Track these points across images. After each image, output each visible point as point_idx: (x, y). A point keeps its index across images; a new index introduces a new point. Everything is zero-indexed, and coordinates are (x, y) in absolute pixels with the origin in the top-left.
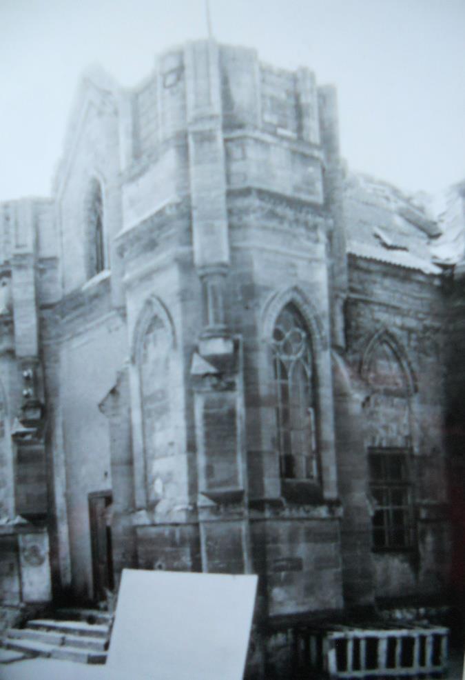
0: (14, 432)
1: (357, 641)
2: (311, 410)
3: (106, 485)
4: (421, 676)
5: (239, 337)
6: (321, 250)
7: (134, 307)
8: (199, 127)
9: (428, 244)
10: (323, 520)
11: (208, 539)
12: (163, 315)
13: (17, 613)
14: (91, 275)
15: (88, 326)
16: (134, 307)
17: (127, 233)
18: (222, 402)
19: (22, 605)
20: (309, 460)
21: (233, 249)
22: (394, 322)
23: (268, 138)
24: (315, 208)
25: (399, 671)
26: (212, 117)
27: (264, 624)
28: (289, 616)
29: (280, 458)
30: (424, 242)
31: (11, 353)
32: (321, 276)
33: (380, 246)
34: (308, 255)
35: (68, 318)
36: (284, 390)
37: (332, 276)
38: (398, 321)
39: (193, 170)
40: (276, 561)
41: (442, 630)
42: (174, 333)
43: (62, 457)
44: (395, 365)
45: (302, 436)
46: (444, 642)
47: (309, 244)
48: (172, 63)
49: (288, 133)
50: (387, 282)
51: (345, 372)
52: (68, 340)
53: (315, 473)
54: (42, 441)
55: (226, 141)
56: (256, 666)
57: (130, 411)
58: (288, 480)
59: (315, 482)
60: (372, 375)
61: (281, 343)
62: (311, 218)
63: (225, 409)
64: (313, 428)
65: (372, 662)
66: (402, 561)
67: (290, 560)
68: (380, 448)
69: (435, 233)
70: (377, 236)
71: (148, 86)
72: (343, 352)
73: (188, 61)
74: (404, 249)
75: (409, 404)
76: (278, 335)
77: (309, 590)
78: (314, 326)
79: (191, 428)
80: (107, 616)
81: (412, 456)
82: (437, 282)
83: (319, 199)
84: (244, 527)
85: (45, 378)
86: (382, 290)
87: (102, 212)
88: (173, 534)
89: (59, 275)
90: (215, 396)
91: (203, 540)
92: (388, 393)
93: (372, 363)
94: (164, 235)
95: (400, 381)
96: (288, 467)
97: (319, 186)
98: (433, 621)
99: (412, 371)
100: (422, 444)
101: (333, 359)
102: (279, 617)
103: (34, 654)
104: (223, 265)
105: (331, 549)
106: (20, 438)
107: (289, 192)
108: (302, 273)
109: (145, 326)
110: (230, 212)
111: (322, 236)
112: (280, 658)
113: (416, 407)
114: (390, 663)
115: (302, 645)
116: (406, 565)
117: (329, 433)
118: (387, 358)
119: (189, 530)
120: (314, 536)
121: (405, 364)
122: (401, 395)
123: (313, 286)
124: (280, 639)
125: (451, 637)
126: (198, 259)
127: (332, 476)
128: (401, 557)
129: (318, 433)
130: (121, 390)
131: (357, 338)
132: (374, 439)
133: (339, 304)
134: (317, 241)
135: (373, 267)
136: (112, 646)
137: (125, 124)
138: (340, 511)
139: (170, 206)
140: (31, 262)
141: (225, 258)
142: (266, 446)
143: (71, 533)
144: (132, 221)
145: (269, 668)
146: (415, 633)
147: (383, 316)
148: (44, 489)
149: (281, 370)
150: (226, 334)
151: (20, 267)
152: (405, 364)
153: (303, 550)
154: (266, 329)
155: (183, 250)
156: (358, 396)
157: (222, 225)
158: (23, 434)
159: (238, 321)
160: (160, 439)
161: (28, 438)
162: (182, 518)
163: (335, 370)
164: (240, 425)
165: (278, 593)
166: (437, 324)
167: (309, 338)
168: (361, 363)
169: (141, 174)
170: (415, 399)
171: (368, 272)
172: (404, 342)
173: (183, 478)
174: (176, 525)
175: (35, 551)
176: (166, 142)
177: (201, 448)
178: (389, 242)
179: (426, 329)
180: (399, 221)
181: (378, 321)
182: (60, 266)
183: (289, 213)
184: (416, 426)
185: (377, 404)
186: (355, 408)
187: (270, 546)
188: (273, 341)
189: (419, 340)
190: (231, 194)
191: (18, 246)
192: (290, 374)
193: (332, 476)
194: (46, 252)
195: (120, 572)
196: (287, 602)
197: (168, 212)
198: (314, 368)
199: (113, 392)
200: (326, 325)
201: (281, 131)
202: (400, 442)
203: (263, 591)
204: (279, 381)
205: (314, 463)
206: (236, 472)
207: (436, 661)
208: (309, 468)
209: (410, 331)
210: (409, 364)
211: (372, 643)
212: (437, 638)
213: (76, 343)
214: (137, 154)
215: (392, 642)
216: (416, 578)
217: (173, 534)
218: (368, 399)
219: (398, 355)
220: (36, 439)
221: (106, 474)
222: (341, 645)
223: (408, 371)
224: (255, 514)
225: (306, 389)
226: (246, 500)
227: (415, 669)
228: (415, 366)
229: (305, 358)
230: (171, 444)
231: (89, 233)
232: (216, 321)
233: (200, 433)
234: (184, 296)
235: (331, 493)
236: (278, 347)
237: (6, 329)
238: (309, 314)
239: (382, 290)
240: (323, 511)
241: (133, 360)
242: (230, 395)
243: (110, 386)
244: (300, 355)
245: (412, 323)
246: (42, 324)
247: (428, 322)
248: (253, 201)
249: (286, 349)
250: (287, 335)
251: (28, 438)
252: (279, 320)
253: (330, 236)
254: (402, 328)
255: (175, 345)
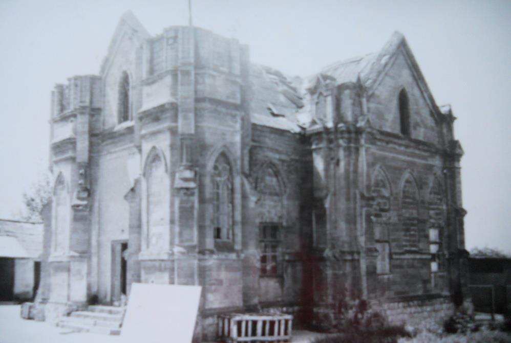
0: (73, 204)
1: (247, 322)
2: (230, 205)
3: (125, 237)
4: (279, 341)
5: (197, 169)
6: (238, 126)
7: (147, 147)
8: (184, 68)
9: (297, 112)
10: (234, 260)
11: (178, 268)
12: (161, 155)
13: (67, 307)
14: (120, 122)
15: (117, 149)
16: (147, 147)
17: (145, 112)
18: (187, 201)
19: (70, 303)
20: (228, 230)
21: (197, 127)
22: (275, 157)
23: (215, 74)
24: (236, 107)
25: (268, 338)
26: (190, 64)
27: (204, 313)
28: (215, 309)
29: (215, 229)
30: (294, 111)
31: (73, 159)
32: (238, 139)
33: (270, 115)
34: (232, 129)
35: (105, 143)
36: (218, 194)
37: (243, 138)
38: (277, 156)
39: (180, 88)
40: (210, 280)
41: (289, 317)
42: (166, 165)
43: (97, 219)
44: (274, 180)
45: (226, 218)
46: (290, 323)
47: (231, 123)
48: (172, 34)
49: (225, 69)
50: (273, 136)
51: (248, 187)
52: (105, 155)
53: (231, 236)
54: (88, 210)
55: (196, 74)
56: (198, 334)
57: (141, 200)
58: (218, 240)
59: (230, 241)
60: (263, 184)
61: (217, 172)
62: (234, 112)
63: (189, 205)
64: (231, 214)
65: (254, 333)
66: (275, 282)
67: (216, 280)
68: (266, 223)
69: (300, 105)
70: (270, 109)
71: (160, 39)
72: (247, 176)
73: (180, 36)
74: (283, 116)
75: (280, 201)
76: (216, 168)
77: (226, 296)
78: (233, 164)
79: (172, 213)
80: (121, 309)
81: (282, 227)
82: (298, 137)
83: (238, 102)
84: (196, 262)
85: (91, 175)
86: (269, 141)
87: (128, 90)
88: (160, 266)
89: (102, 118)
90: (185, 198)
91: (176, 268)
92: (271, 194)
93: (263, 179)
94: (164, 116)
95: (277, 188)
96: (218, 233)
97: (238, 96)
98: (288, 313)
99: (284, 183)
100: (287, 221)
101: (242, 179)
102: (210, 309)
103: (79, 330)
104: (191, 135)
105: (238, 275)
106: (76, 208)
107: (223, 98)
108: (228, 138)
109: (150, 159)
110: (196, 109)
111: (239, 121)
112: (211, 329)
113: (285, 202)
114: (263, 334)
115: (221, 325)
116: (277, 284)
117: (238, 217)
118: (270, 175)
119: (169, 264)
120: (229, 268)
121: (280, 178)
122: (277, 195)
123: (233, 144)
124: (210, 321)
125: (293, 320)
126: (180, 130)
127: (239, 238)
128: (275, 280)
129: (233, 217)
130: (137, 190)
131: (256, 165)
132: (262, 218)
133: (246, 152)
134: (236, 122)
135: (265, 129)
136: (124, 326)
137: (146, 55)
138: (243, 256)
139: (168, 104)
140: (88, 110)
141: (193, 131)
142: (208, 223)
143: (99, 264)
144: (149, 104)
145: (205, 337)
146: (276, 318)
147: (271, 155)
148: (87, 237)
149: (216, 185)
150: (190, 168)
151: (82, 113)
152: (280, 178)
153: (224, 275)
154: (210, 165)
155: (173, 125)
156: (253, 199)
157: (191, 116)
158: (78, 206)
159: (197, 161)
160: (155, 217)
161: (81, 208)
162: (165, 257)
163: (243, 185)
164: (196, 213)
165: (210, 297)
166: (297, 158)
167: (231, 171)
168: (257, 179)
169: (153, 82)
170: (285, 197)
171: (261, 131)
172: (280, 167)
173: (167, 237)
174: (163, 260)
175: (79, 272)
176: (167, 72)
177: (177, 223)
178: (276, 112)
179: (292, 160)
180: (282, 99)
181: (267, 157)
182: (102, 114)
183: (224, 110)
184: (285, 213)
185: (264, 200)
186: (252, 204)
187: (208, 273)
188: (213, 171)
189: (289, 166)
190: (197, 100)
191: (81, 102)
192: (221, 187)
193: (239, 238)
194: (97, 105)
195: (130, 284)
196: (216, 301)
197: (167, 106)
198: (232, 184)
199: (133, 190)
200: (239, 162)
201: (222, 69)
202: (276, 220)
203: (203, 296)
204: (215, 190)
205: (231, 232)
206: (193, 237)
207: (286, 333)
208: (228, 234)
209: (283, 161)
210: (282, 179)
211: (255, 323)
212: (287, 321)
213: (109, 157)
214: (152, 71)
215: (264, 323)
216: (282, 291)
217: (160, 266)
218: (259, 200)
219: (276, 174)
220: (84, 209)
221: (123, 231)
222: (239, 324)
223: (281, 182)
224: (201, 257)
225: (228, 194)
226: (197, 250)
227: (275, 337)
228: (286, 180)
229: (228, 179)
230: (162, 219)
231: (120, 99)
232: (187, 161)
233: (177, 215)
234: (172, 147)
235: (238, 247)
236: (215, 174)
237: (71, 146)
238: (231, 158)
239: (269, 141)
240: (233, 256)
241: (144, 175)
242: (191, 198)
243: (132, 185)
244: (226, 177)
245: (284, 157)
246: (91, 145)
247: (293, 157)
248: (207, 105)
249: (219, 175)
250: (220, 168)
251: (81, 208)
252: (217, 161)
253: (243, 119)
254: (280, 160)
255: (166, 171)
